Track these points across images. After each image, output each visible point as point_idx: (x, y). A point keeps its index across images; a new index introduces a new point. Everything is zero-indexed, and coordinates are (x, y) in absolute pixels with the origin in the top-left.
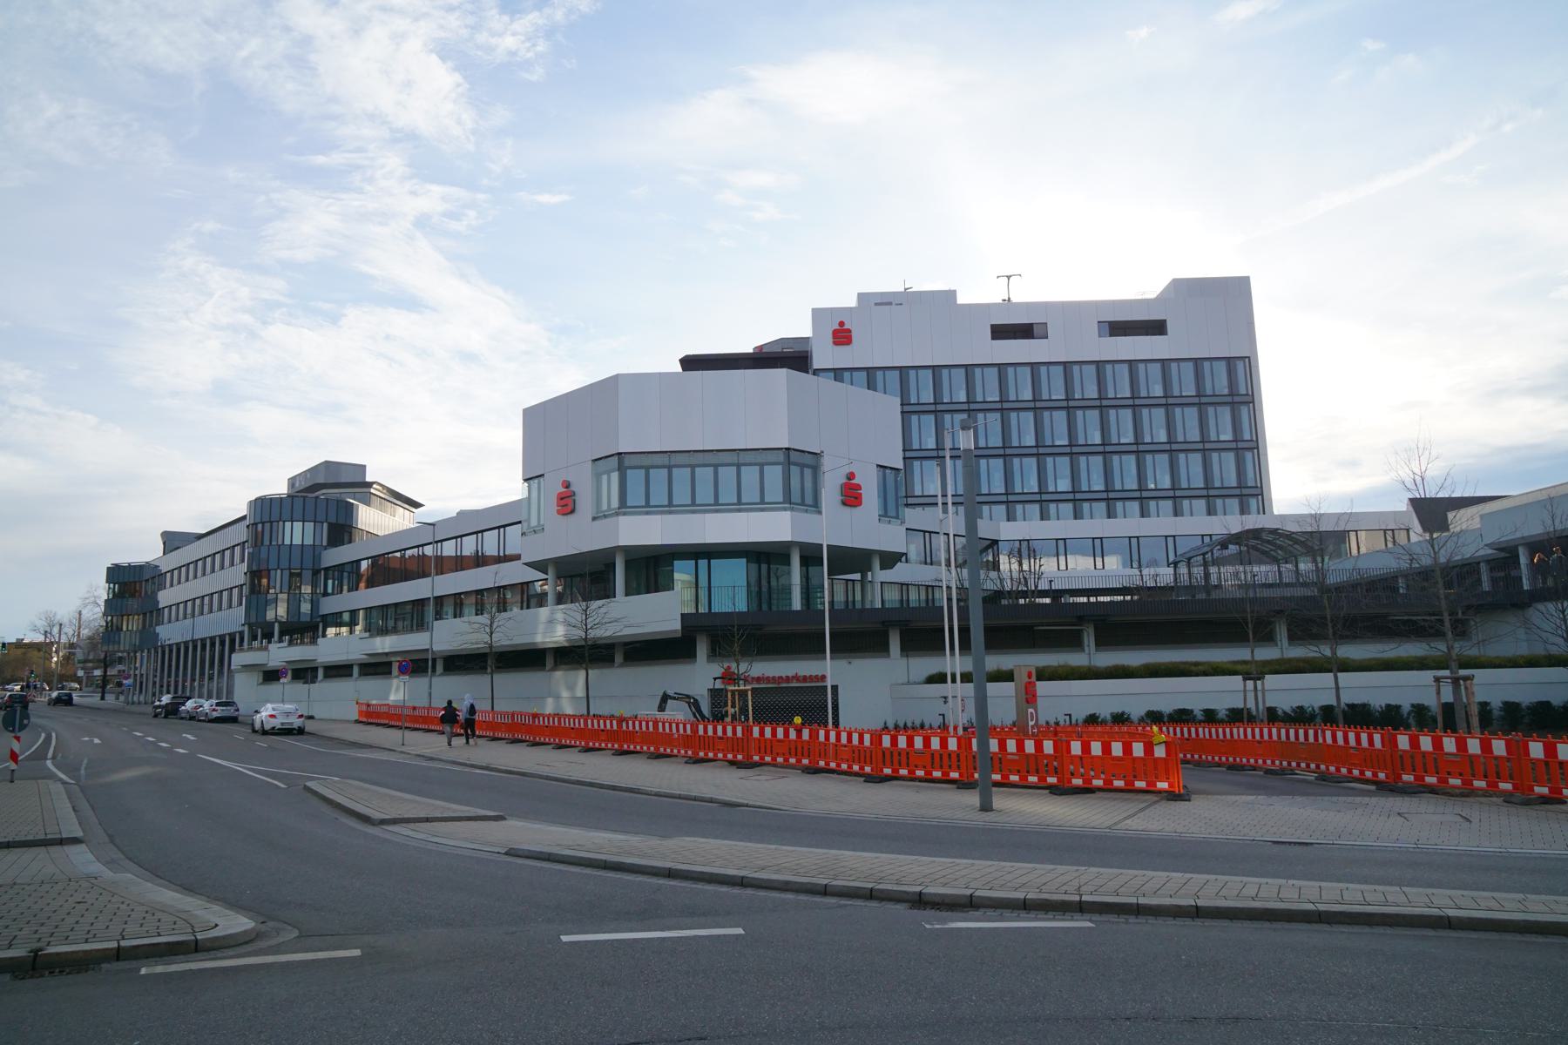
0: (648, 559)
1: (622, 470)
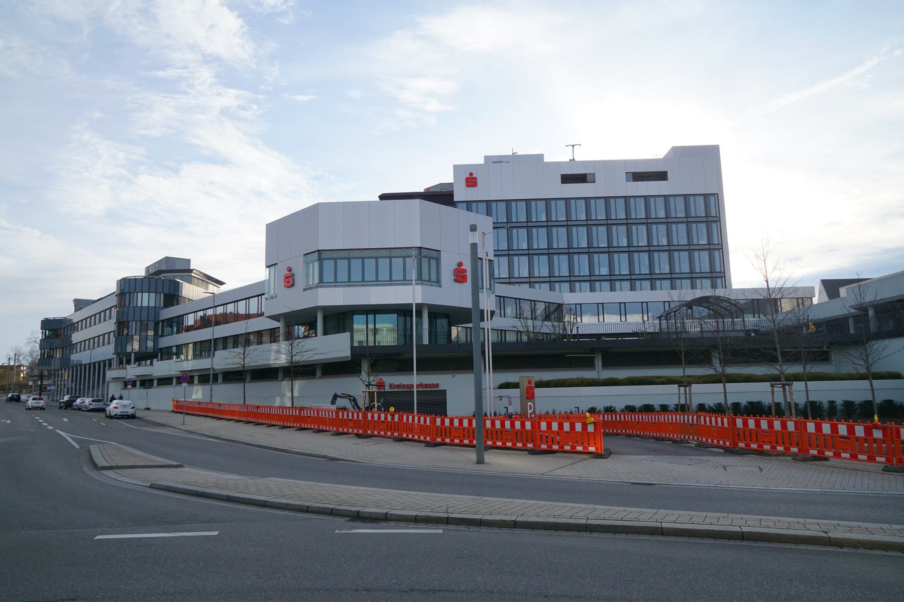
0: (339, 314)
1: (320, 260)
